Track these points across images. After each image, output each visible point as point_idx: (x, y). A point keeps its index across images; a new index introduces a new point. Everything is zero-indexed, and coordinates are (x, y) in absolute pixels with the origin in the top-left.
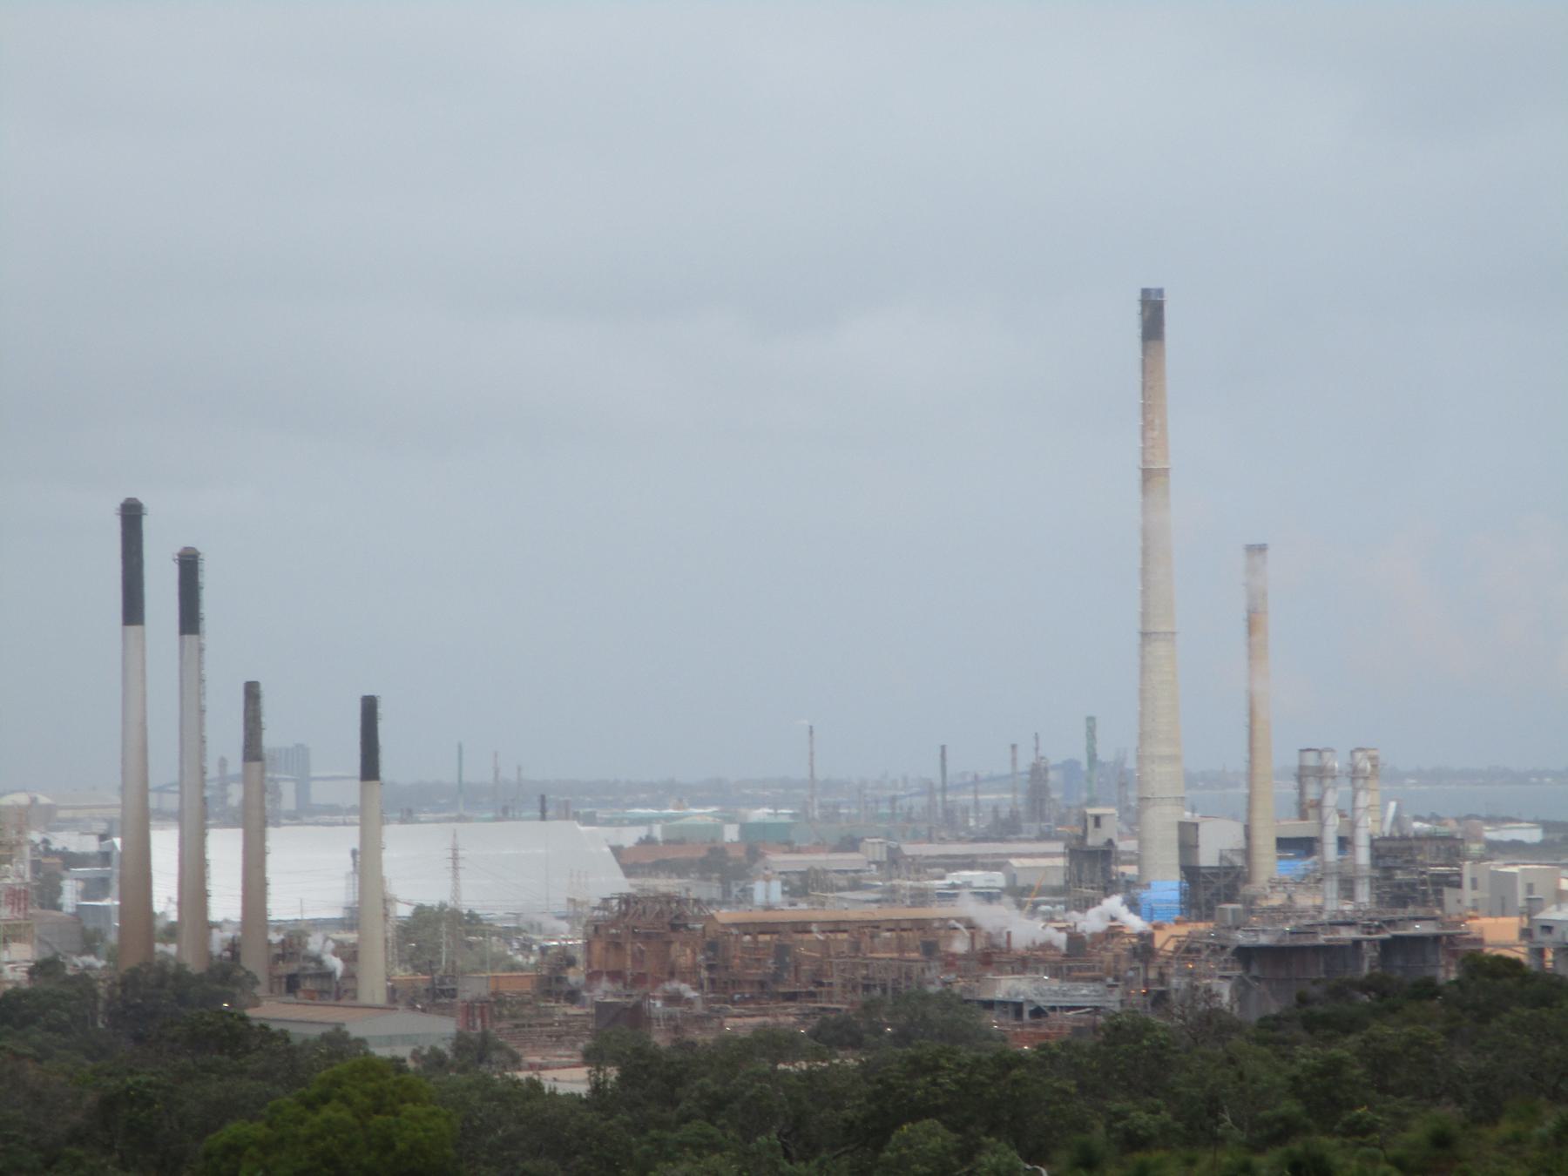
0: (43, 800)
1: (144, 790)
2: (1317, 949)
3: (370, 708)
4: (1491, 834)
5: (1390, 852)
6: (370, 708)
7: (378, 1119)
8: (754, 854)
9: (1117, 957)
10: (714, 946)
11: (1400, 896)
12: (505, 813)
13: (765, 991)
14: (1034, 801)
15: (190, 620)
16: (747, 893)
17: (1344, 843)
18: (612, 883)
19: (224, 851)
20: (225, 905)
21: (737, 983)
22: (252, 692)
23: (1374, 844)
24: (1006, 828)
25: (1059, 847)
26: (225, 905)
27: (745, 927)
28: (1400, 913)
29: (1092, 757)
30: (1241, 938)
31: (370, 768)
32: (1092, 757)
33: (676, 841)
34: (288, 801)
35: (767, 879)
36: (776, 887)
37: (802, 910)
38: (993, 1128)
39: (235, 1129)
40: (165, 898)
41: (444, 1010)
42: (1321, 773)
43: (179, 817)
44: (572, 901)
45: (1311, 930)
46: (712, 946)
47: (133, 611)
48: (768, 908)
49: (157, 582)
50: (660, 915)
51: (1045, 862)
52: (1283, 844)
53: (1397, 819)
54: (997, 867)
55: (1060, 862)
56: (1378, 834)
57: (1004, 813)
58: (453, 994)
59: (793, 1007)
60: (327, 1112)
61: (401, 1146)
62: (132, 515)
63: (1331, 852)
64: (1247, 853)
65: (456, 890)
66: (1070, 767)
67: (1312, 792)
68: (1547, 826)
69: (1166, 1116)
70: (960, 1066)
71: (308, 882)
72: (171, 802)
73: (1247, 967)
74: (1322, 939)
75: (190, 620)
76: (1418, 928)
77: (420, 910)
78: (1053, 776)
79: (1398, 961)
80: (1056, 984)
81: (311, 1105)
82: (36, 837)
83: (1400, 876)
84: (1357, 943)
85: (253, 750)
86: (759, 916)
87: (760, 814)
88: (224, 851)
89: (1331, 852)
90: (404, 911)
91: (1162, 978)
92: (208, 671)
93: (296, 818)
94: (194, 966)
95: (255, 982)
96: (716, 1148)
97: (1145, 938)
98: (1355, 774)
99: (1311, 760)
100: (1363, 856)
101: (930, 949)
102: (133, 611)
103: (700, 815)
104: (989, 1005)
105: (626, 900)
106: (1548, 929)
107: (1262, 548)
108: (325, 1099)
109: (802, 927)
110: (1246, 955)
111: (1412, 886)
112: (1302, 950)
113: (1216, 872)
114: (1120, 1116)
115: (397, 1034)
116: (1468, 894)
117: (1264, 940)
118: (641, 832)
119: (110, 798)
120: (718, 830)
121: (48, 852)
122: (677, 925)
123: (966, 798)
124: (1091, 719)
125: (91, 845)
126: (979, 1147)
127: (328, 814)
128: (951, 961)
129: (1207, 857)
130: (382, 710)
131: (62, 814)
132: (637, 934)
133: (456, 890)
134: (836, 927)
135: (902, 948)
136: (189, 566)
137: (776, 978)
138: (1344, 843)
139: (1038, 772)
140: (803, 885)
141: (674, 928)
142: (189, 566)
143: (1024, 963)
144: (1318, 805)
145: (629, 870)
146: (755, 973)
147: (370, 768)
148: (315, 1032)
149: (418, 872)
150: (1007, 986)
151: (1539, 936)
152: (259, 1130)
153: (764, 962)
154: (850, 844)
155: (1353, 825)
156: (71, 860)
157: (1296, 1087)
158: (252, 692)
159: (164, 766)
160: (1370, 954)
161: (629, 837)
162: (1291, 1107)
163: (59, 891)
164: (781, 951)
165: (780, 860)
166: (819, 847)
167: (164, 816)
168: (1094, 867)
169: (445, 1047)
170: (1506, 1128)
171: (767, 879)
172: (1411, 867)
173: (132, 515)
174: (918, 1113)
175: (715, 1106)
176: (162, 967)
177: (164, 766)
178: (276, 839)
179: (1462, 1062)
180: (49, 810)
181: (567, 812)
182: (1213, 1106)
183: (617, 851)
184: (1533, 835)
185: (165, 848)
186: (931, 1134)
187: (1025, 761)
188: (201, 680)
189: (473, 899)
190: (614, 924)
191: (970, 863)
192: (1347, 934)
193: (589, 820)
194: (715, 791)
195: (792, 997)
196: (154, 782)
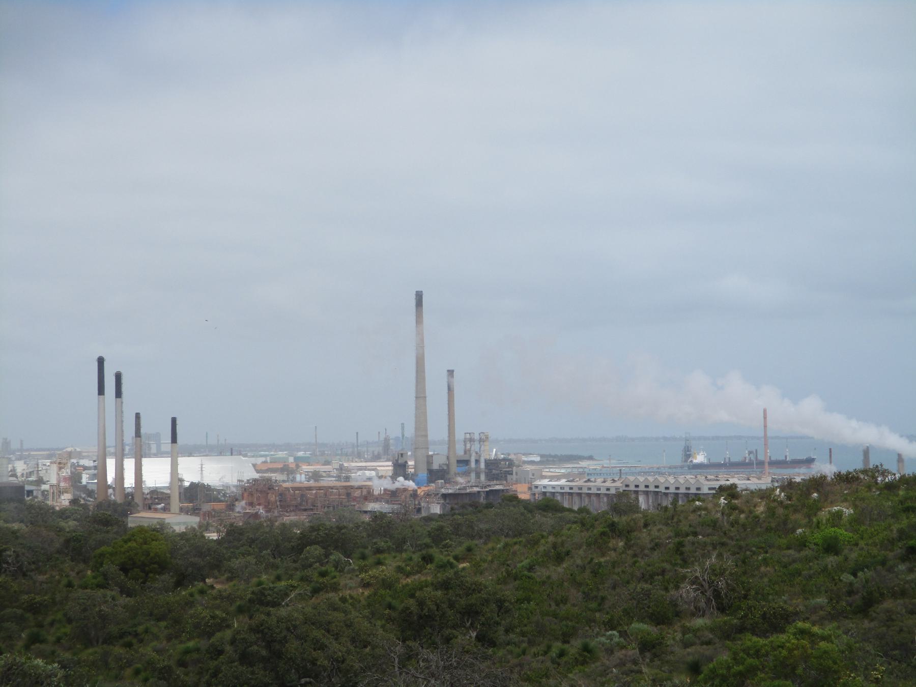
0: (78, 450)
1: (105, 448)
2: (466, 494)
3: (174, 421)
4: (524, 458)
5: (492, 465)
6: (174, 421)
7: (145, 547)
8: (298, 466)
9: (406, 497)
10: (282, 494)
11: (491, 477)
12: (221, 453)
13: (298, 508)
14: (384, 450)
15: (119, 394)
16: (294, 478)
17: (477, 461)
18: (252, 475)
19: (129, 465)
20: (129, 482)
21: (289, 506)
22: (138, 416)
23: (486, 461)
24: (377, 458)
25: (390, 463)
26: (129, 482)
27: (295, 489)
28: (492, 483)
29: (403, 436)
30: (443, 491)
31: (174, 440)
32: (403, 436)
33: (274, 461)
34: (154, 449)
35: (301, 474)
36: (303, 476)
37: (312, 483)
38: (336, 548)
39: (103, 548)
40: (111, 477)
41: (197, 515)
42: (471, 440)
43: (115, 454)
44: (239, 481)
45: (465, 488)
46: (281, 495)
47: (101, 391)
48: (301, 482)
49: (107, 381)
50: (265, 485)
51: (386, 467)
52: (459, 462)
53: (496, 454)
54: (373, 470)
55: (391, 468)
56: (488, 457)
57: (376, 453)
58: (200, 509)
59: (305, 513)
60: (129, 544)
61: (152, 555)
62: (101, 361)
63: (473, 465)
64: (448, 465)
65: (202, 477)
66: (397, 439)
67: (468, 446)
68: (542, 456)
69: (390, 544)
70: (326, 529)
71: (157, 474)
72: (112, 450)
73: (445, 500)
74: (468, 491)
75: (119, 394)
76: (497, 487)
77: (192, 484)
78: (391, 441)
79: (491, 497)
80: (386, 506)
81: (126, 542)
82: (74, 461)
83: (494, 471)
84: (479, 492)
85: (138, 434)
86: (296, 485)
87: (301, 454)
88: (129, 465)
89: (473, 465)
90: (187, 484)
91: (419, 504)
92: (124, 409)
93: (156, 455)
94: (119, 500)
95: (138, 506)
96: (249, 554)
97: (415, 491)
98: (481, 440)
99: (468, 436)
100: (482, 465)
101: (348, 495)
102: (101, 391)
103: (281, 454)
104: (366, 512)
105: (255, 480)
106: (536, 487)
107: (453, 371)
108: (130, 540)
109: (310, 488)
110: (445, 496)
111: (498, 475)
112: (462, 494)
113: (438, 471)
114: (375, 543)
115: (179, 522)
116: (514, 477)
117: (450, 491)
118: (263, 459)
119: (94, 449)
120: (287, 459)
121: (79, 466)
122: (271, 488)
123: (365, 449)
124: (403, 424)
125: (91, 464)
126: (331, 554)
127: (159, 454)
128: (355, 499)
129: (435, 466)
130: (178, 422)
131: (84, 454)
132: (258, 490)
133: (202, 477)
134: (320, 488)
135: (339, 495)
136: (118, 377)
137: (301, 504)
138: (477, 461)
139: (387, 440)
140: (316, 476)
141: (269, 489)
142: (118, 377)
143: (377, 499)
144: (470, 450)
145: (258, 471)
146: (294, 502)
147: (174, 440)
148: (155, 522)
149: (193, 470)
150: (372, 506)
151: (534, 489)
152: (109, 549)
153: (297, 499)
154: (327, 463)
155: (480, 456)
156: (85, 468)
157: (429, 534)
158: (138, 416)
159: (111, 440)
160: (483, 495)
161: (259, 461)
162: (428, 540)
163: (81, 478)
164: (302, 496)
165: (305, 468)
166: (318, 463)
167: (111, 454)
168: (400, 468)
169: (195, 526)
170: (490, 545)
171: (301, 474)
172: (498, 469)
173: (101, 361)
174: (311, 544)
175: (252, 541)
176: (109, 501)
177: (111, 440)
178: (145, 461)
179: (482, 526)
180: (80, 453)
181: (240, 453)
182: (404, 541)
183: (254, 465)
184: (538, 459)
185: (111, 464)
186: (316, 549)
187: (382, 438)
188: (122, 412)
189: (206, 481)
190: (250, 487)
191: (365, 468)
192: (476, 489)
193: (245, 456)
194: (288, 447)
195: (305, 510)
196: (107, 444)
